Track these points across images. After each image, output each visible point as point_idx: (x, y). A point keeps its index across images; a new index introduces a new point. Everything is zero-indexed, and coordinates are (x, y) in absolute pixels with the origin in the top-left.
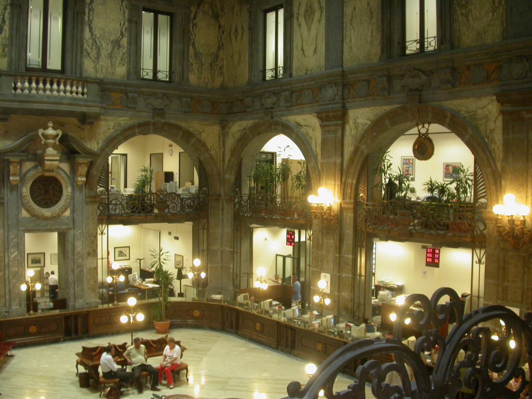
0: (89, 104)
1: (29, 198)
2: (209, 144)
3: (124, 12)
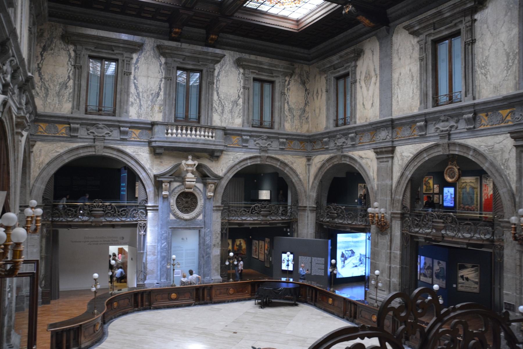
0: (216, 143)
1: (175, 207)
2: (298, 171)
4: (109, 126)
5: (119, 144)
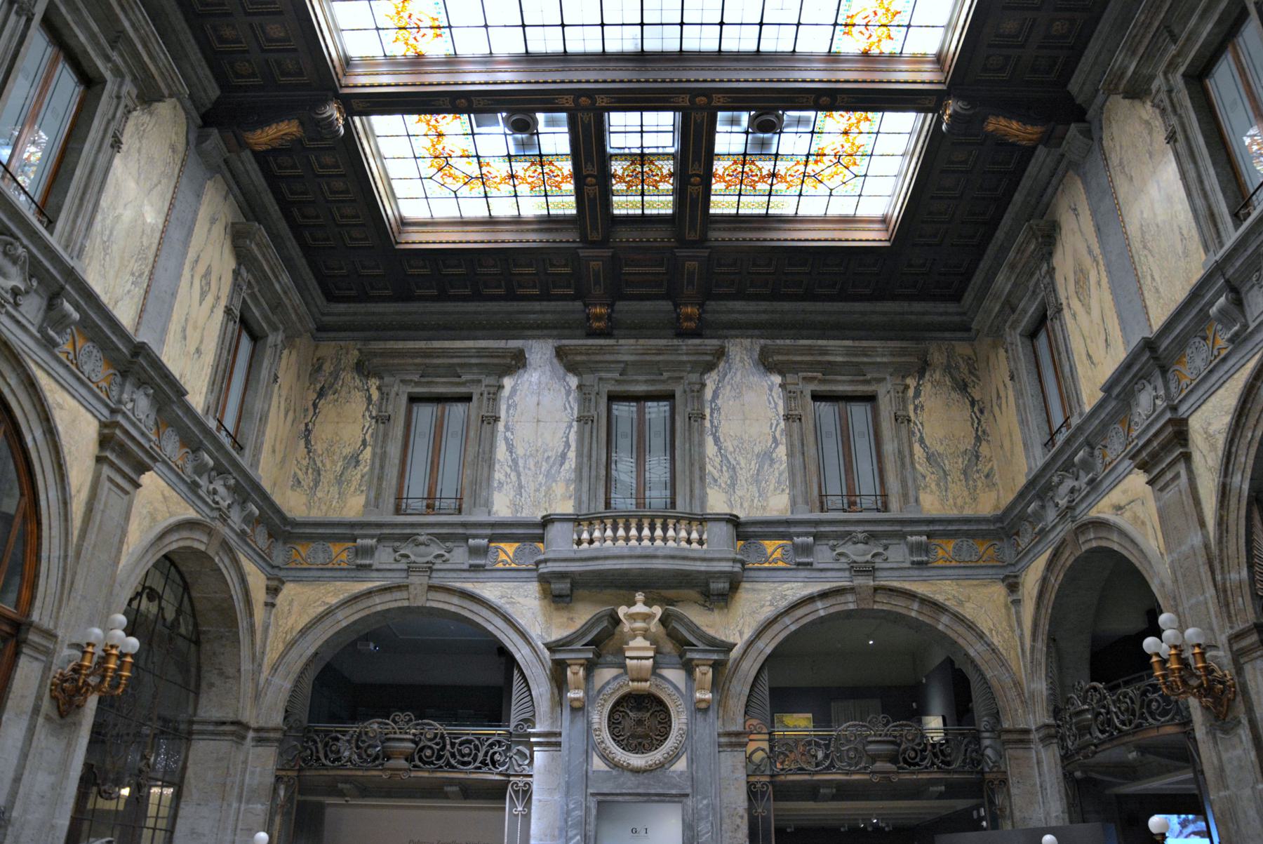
2: (984, 625)
3: (776, 404)
4: (443, 538)
5: (466, 580)
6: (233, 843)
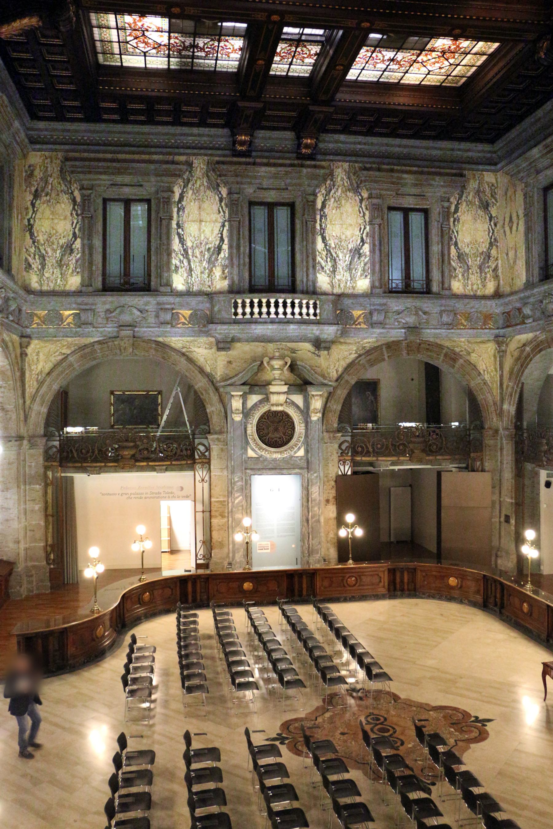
3: (364, 214)
6: (1, 387)
